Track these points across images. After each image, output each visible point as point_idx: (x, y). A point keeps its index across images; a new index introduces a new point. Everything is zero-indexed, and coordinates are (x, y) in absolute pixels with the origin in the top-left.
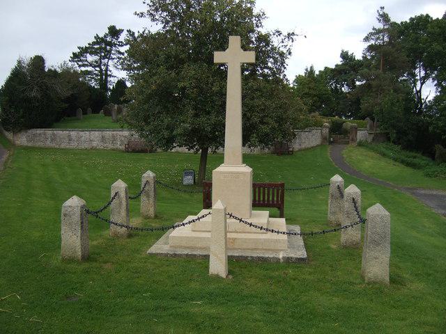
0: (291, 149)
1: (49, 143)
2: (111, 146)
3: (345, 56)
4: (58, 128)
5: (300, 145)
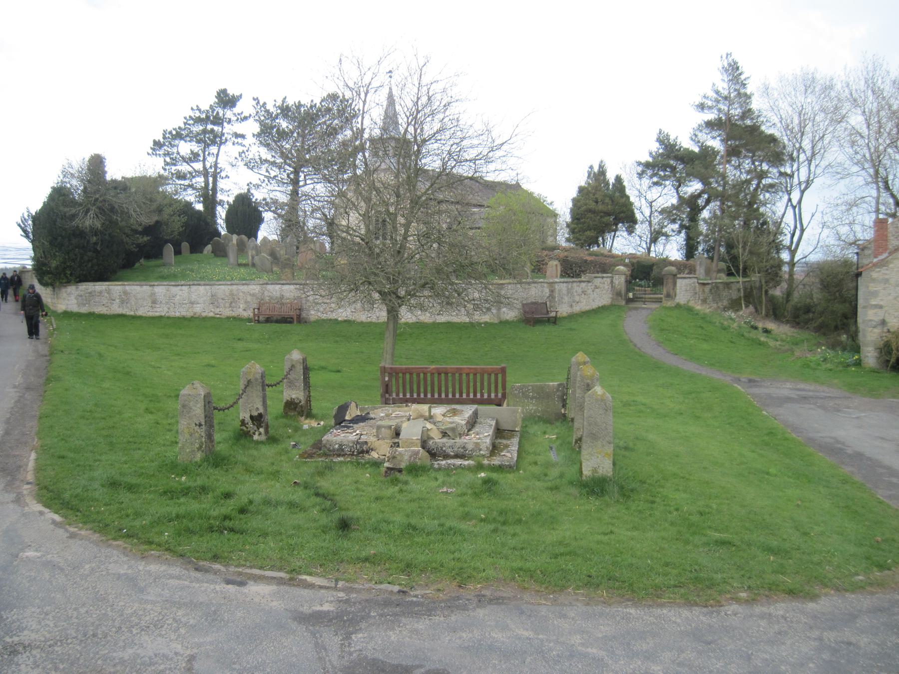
0: (553, 314)
1: (116, 309)
2: (227, 312)
3: (663, 140)
4: (127, 280)
5: (571, 306)
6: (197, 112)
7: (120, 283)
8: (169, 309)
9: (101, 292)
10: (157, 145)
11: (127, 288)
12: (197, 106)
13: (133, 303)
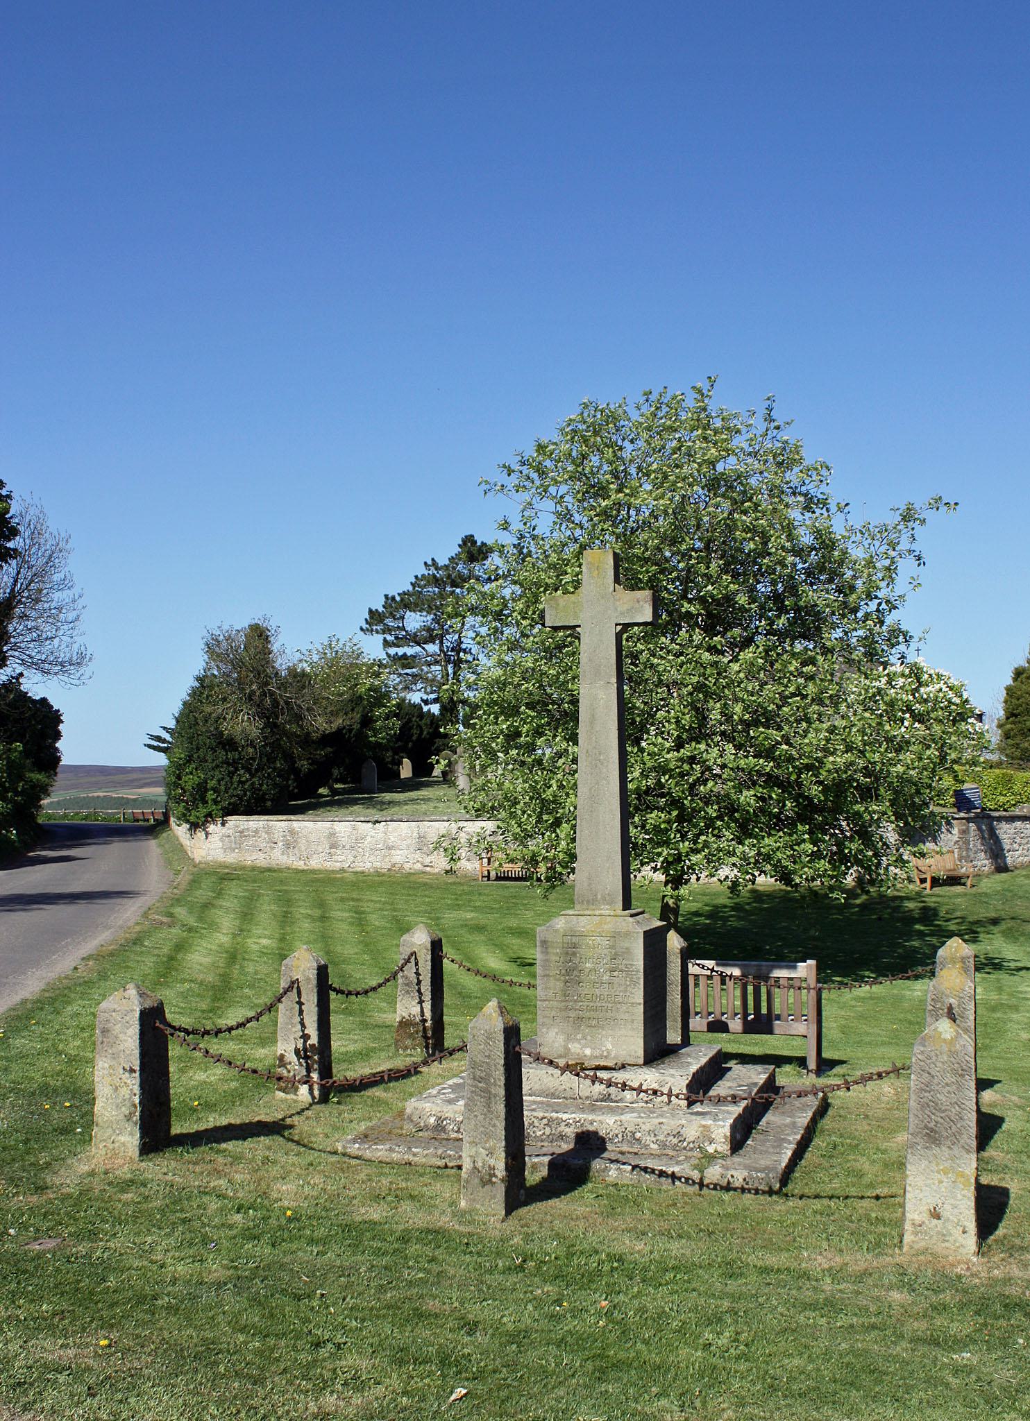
6: (432, 568)
7: (285, 817)
8: (355, 857)
9: (256, 831)
10: (375, 617)
11: (295, 824)
12: (433, 560)
13: (303, 849)
